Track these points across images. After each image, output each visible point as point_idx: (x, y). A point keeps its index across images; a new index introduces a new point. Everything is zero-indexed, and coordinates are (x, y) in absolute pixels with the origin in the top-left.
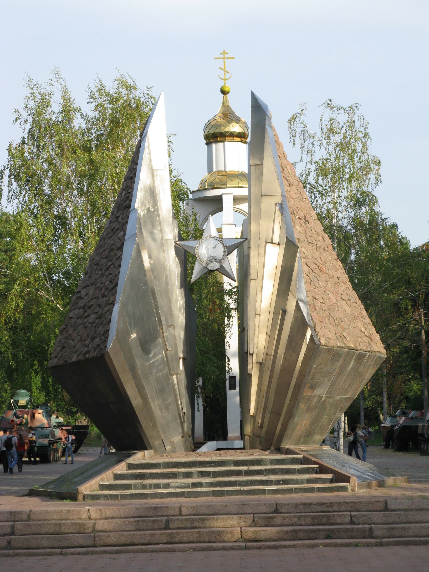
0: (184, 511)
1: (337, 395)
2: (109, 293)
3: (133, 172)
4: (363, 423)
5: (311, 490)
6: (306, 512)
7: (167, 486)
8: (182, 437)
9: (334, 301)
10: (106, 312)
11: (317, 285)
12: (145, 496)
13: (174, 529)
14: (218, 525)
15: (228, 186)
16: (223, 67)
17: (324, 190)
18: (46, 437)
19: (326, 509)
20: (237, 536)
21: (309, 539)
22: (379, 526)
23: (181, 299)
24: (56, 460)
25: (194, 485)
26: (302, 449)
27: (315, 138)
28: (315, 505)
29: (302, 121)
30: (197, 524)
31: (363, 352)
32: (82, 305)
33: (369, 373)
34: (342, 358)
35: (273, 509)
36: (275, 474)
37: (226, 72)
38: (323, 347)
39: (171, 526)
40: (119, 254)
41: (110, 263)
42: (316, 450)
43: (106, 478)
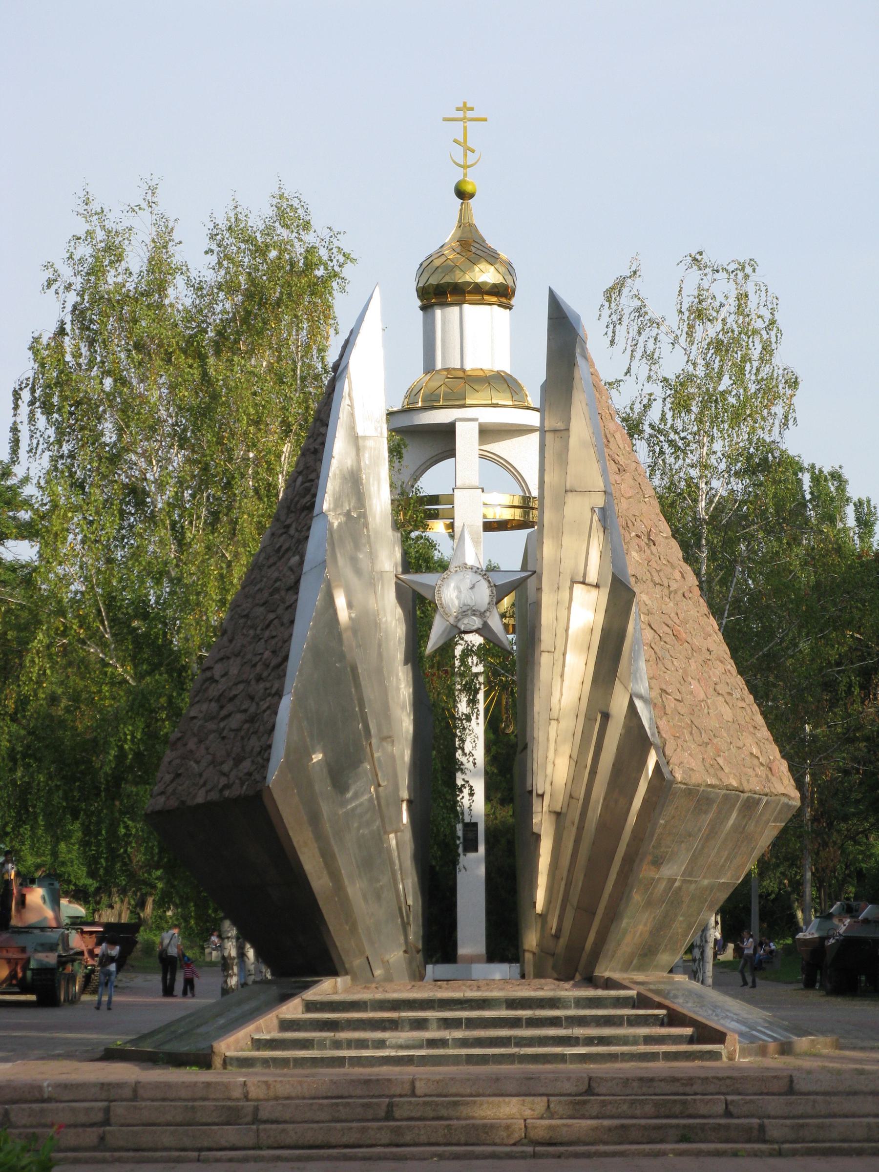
0: (420, 1087)
1: (704, 878)
2: (269, 675)
3: (319, 440)
4: (757, 930)
5: (653, 1057)
6: (644, 1095)
7: (381, 1044)
8: (405, 952)
9: (702, 696)
10: (265, 711)
11: (669, 666)
12: (340, 1061)
13: (402, 1120)
14: (483, 1114)
15: (468, 402)
16: (461, 140)
17: (682, 439)
18: (52, 948)
19: (681, 1090)
20: (518, 1134)
21: (648, 1143)
22: (777, 1121)
23: (406, 686)
24: (73, 1001)
25: (432, 1043)
26: (638, 980)
27: (662, 328)
28: (661, 1081)
29: (635, 292)
30: (444, 1112)
31: (755, 796)
32: (216, 694)
33: (765, 837)
34: (715, 806)
35: (583, 1087)
36: (584, 1026)
37: (468, 149)
38: (679, 785)
40: (290, 598)
41: (271, 616)
42: (660, 982)
43: (265, 1026)
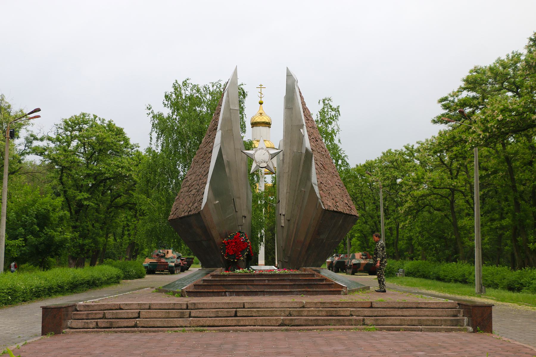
19: (334, 306)
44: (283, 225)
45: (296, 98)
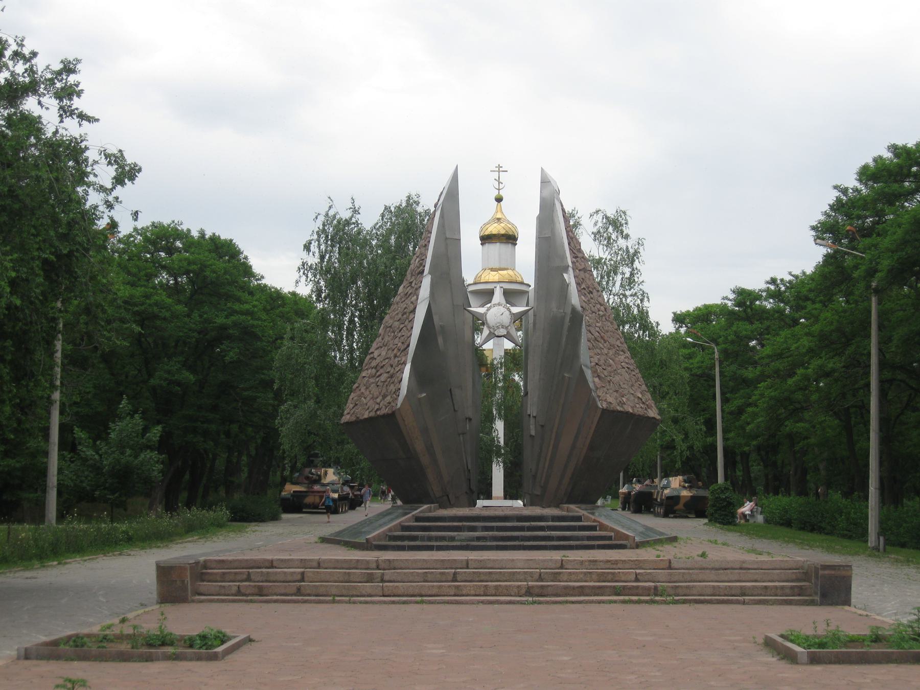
19: (612, 566)
25: (479, 539)
35: (559, 565)
39: (458, 579)
41: (402, 326)
44: (533, 433)
45: (556, 220)
